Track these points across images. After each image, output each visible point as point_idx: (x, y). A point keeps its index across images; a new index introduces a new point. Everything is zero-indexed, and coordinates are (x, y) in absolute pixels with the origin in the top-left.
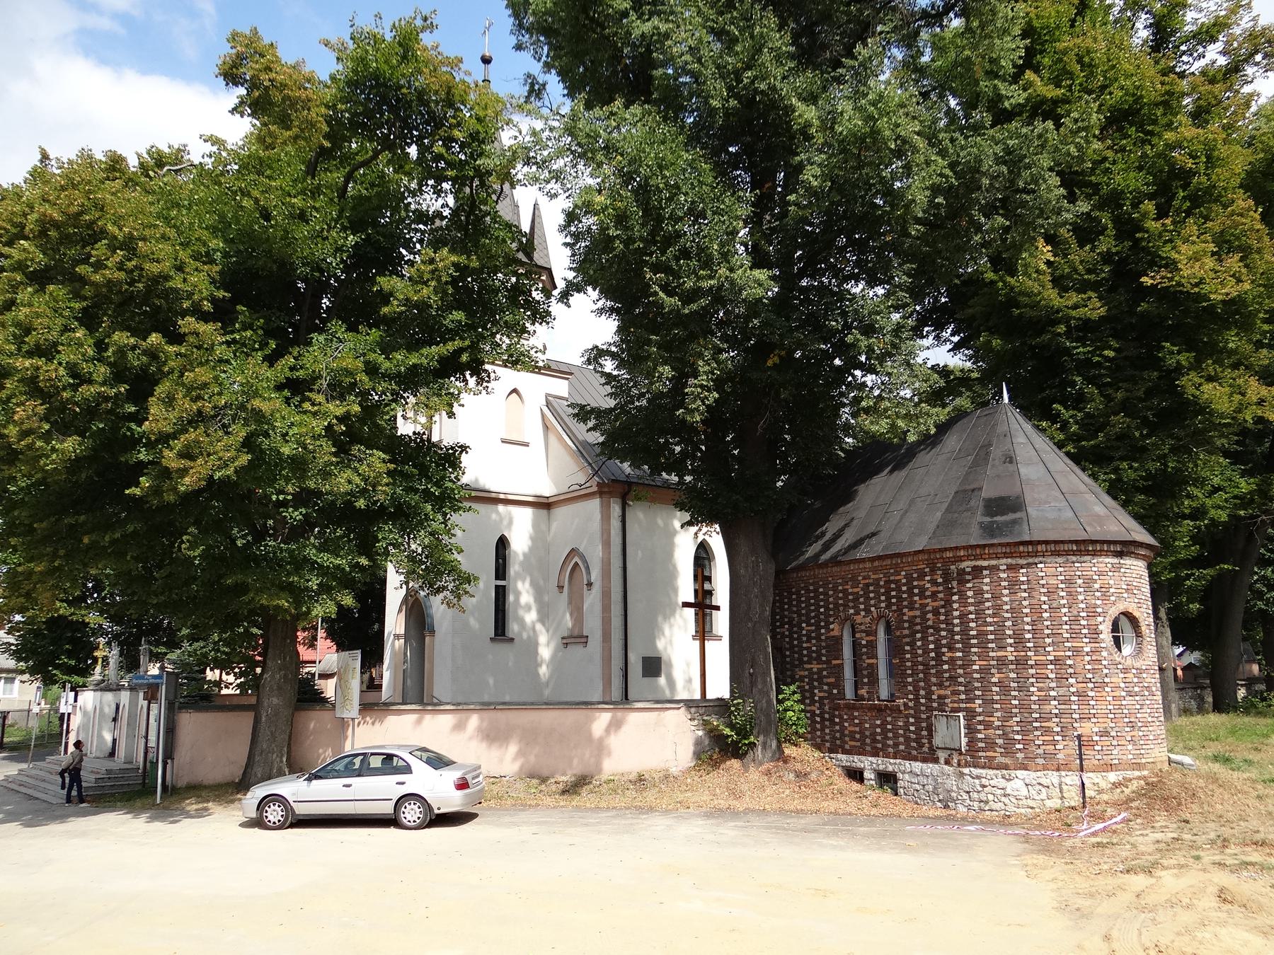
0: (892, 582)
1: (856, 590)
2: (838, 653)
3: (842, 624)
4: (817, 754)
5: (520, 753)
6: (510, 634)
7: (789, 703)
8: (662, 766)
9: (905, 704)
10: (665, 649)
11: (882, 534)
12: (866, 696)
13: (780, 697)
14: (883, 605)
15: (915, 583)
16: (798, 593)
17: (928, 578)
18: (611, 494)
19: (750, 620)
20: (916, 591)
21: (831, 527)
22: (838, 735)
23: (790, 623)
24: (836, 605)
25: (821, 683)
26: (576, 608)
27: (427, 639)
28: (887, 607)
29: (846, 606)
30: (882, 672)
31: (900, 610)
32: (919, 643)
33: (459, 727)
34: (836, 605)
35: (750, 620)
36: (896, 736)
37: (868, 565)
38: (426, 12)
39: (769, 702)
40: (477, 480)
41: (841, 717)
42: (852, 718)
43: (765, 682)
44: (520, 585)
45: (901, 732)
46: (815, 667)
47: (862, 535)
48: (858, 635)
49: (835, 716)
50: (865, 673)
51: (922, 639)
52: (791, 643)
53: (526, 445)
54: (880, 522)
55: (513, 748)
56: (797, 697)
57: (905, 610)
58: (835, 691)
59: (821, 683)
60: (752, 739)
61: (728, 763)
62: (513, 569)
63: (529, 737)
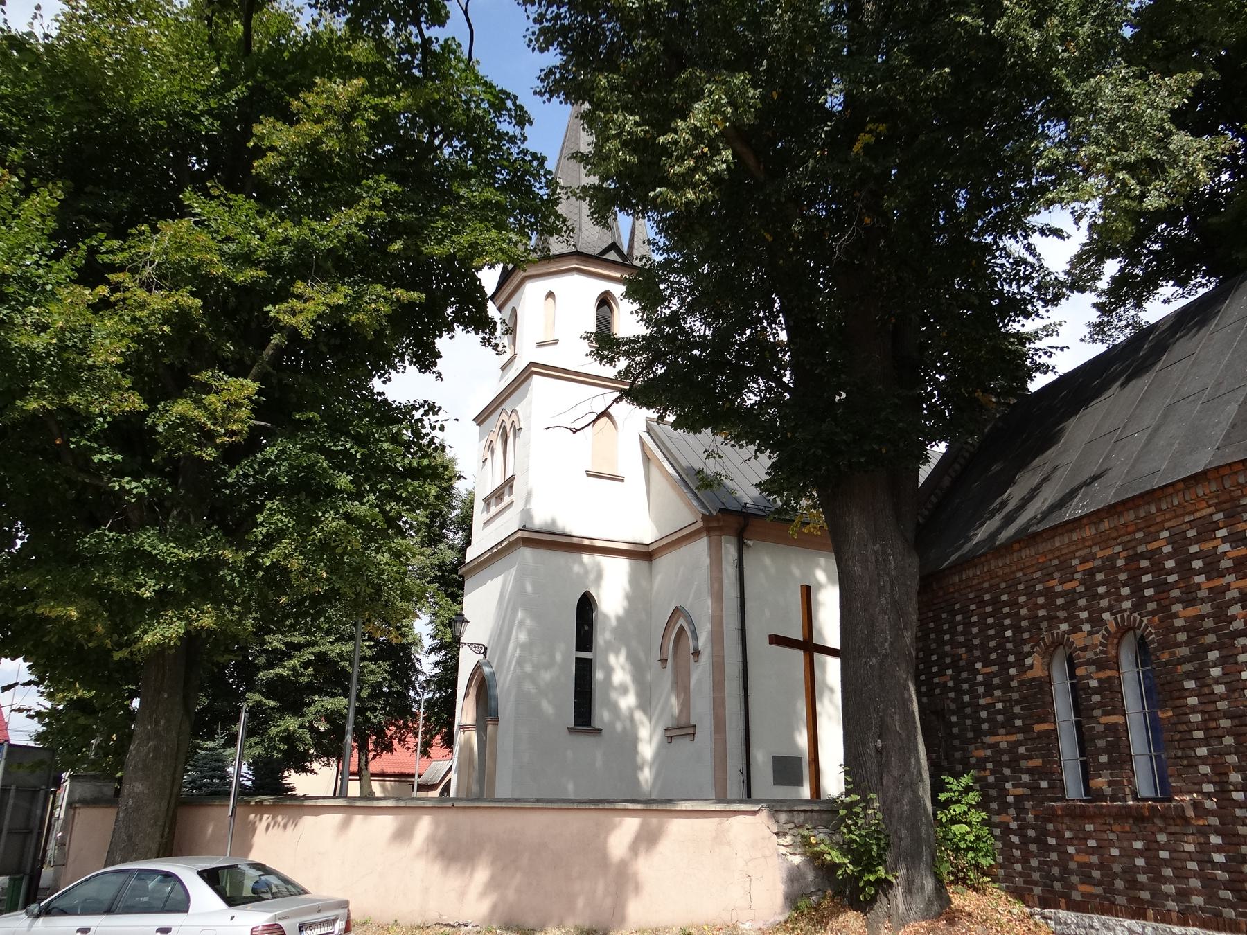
0: (1142, 556)
1: (1068, 586)
2: (1047, 714)
3: (1048, 655)
4: (1018, 908)
5: (493, 884)
6: (596, 723)
7: (958, 809)
8: (726, 917)
9: (1196, 805)
11: (1111, 474)
12: (1107, 790)
13: (942, 797)
14: (1127, 605)
15: (1194, 549)
16: (965, 611)
17: (1222, 533)
18: (721, 530)
19: (874, 651)
20: (1197, 564)
21: (1015, 494)
22: (1056, 871)
23: (955, 665)
24: (1035, 620)
25: (1016, 769)
26: (681, 686)
27: (490, 728)
28: (1136, 607)
29: (1052, 619)
30: (1138, 741)
31: (1164, 610)
32: (1216, 672)
33: (403, 834)
34: (1035, 620)
35: (874, 651)
36: (1181, 875)
37: (1089, 531)
39: (917, 802)
40: (554, 522)
41: (1058, 834)
42: (1082, 838)
43: (905, 766)
44: (612, 659)
45: (1192, 865)
46: (1003, 740)
47: (1075, 484)
48: (1080, 672)
49: (1046, 833)
50: (1101, 743)
51: (1222, 661)
52: (958, 700)
53: (621, 479)
54: (1108, 457)
55: (482, 875)
56: (973, 797)
57: (1177, 608)
58: (1044, 784)
59: (1016, 769)
60: (881, 872)
61: (842, 918)
62: (602, 637)
63: (507, 858)
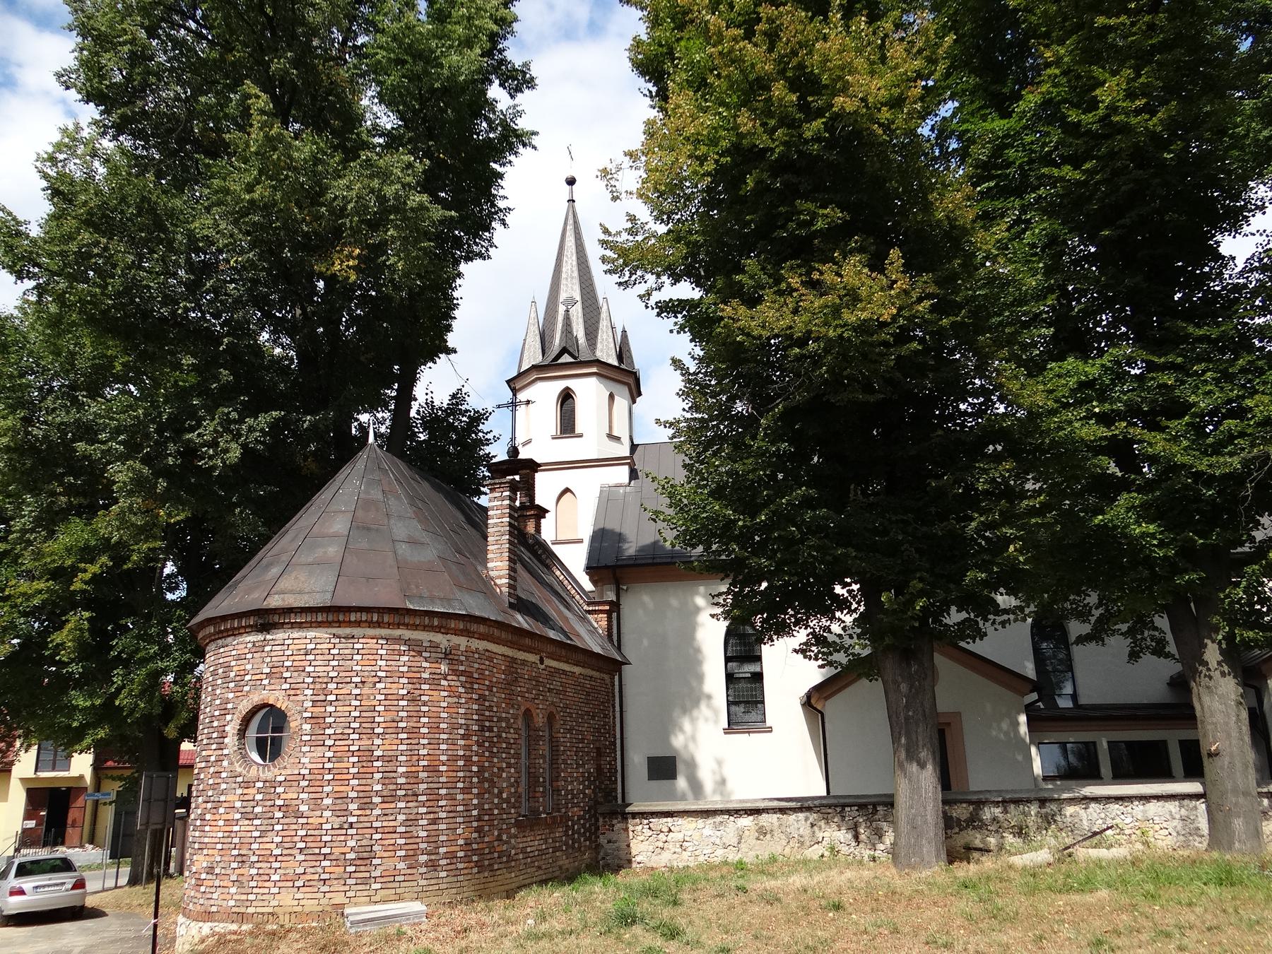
10: (686, 746)
38: (35, 157)
